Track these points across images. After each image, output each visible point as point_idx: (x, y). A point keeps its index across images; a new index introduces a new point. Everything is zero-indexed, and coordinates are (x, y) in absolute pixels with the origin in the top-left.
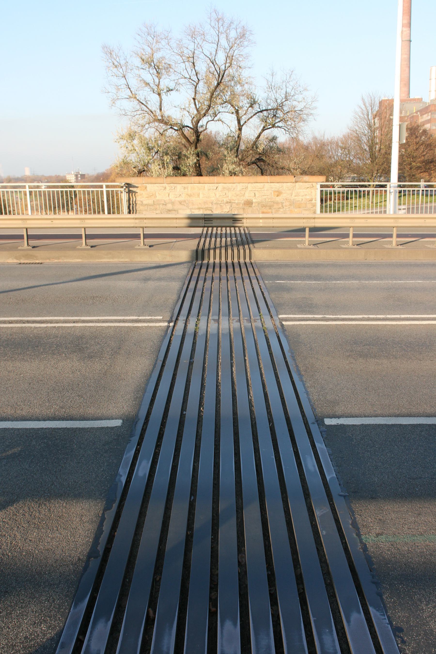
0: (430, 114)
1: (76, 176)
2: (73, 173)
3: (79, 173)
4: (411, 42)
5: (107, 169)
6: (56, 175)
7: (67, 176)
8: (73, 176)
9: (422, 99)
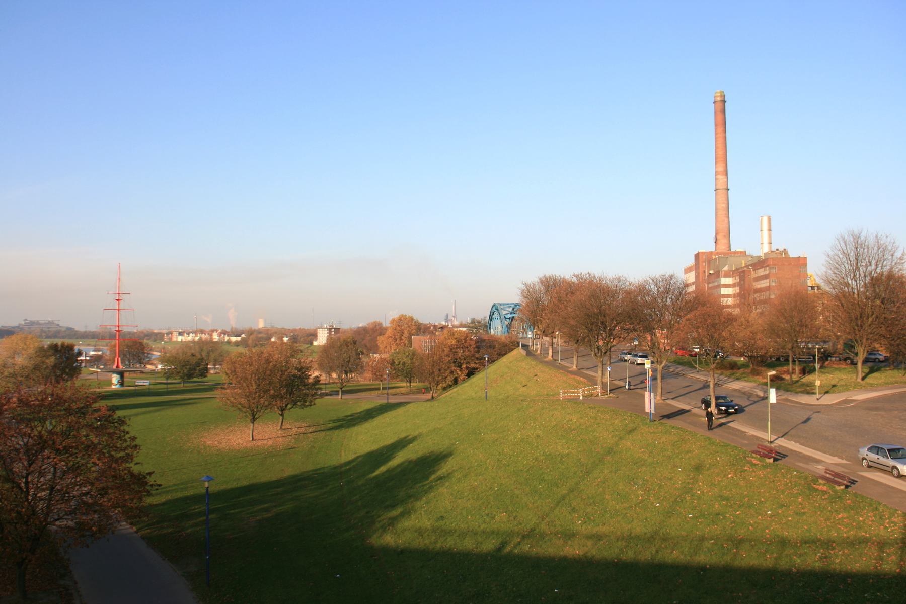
0: (767, 268)
1: (330, 330)
2: (325, 326)
3: (333, 326)
4: (729, 191)
5: (369, 323)
6: (251, 329)
7: (319, 330)
8: (326, 329)
9: (745, 252)
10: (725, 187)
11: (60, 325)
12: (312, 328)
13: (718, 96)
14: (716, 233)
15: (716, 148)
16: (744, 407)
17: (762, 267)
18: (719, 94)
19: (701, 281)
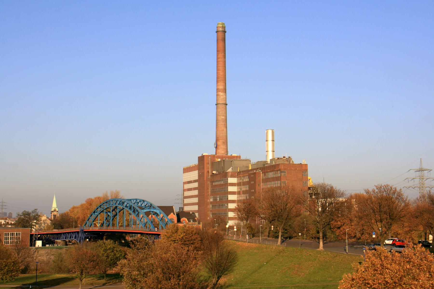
6: (88, 199)
10: (224, 102)
11: (302, 164)
12: (73, 206)
13: (220, 27)
14: (217, 141)
15: (218, 70)
16: (36, 281)
17: (273, 171)
18: (221, 26)
19: (205, 179)
